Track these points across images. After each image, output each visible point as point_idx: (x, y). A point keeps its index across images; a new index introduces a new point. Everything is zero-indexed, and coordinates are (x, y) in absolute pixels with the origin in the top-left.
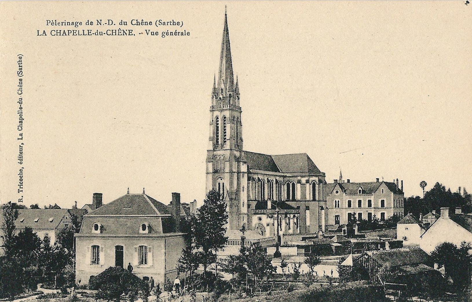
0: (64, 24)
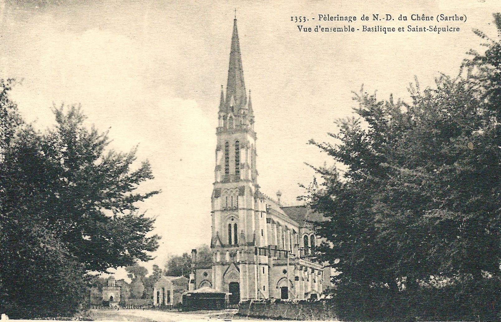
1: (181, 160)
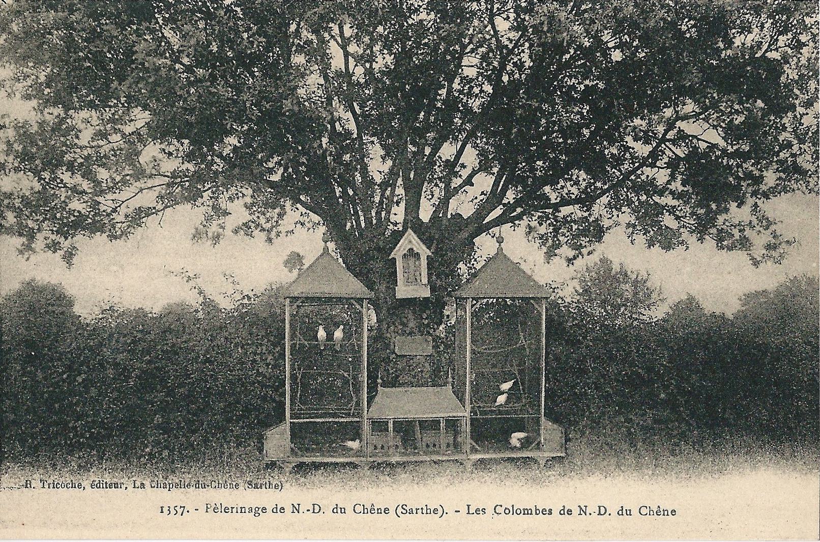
0: (234, 510)
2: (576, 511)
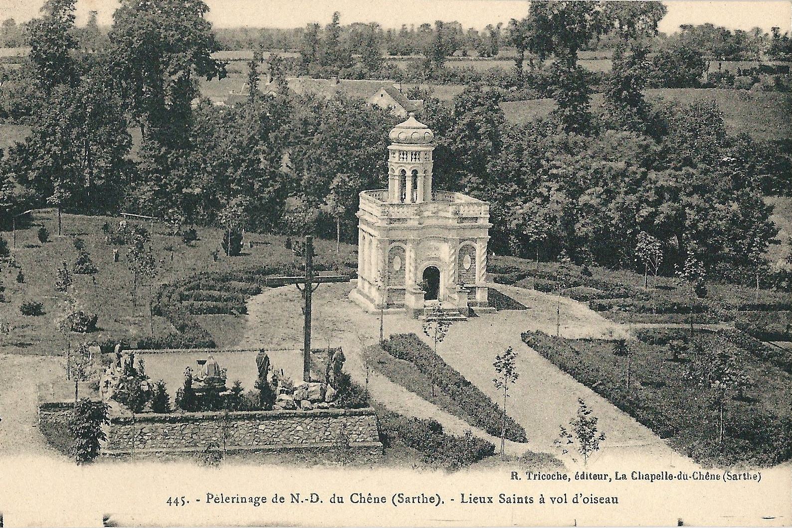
0: (235, 500)
1: (680, 524)
2: (288, 499)
